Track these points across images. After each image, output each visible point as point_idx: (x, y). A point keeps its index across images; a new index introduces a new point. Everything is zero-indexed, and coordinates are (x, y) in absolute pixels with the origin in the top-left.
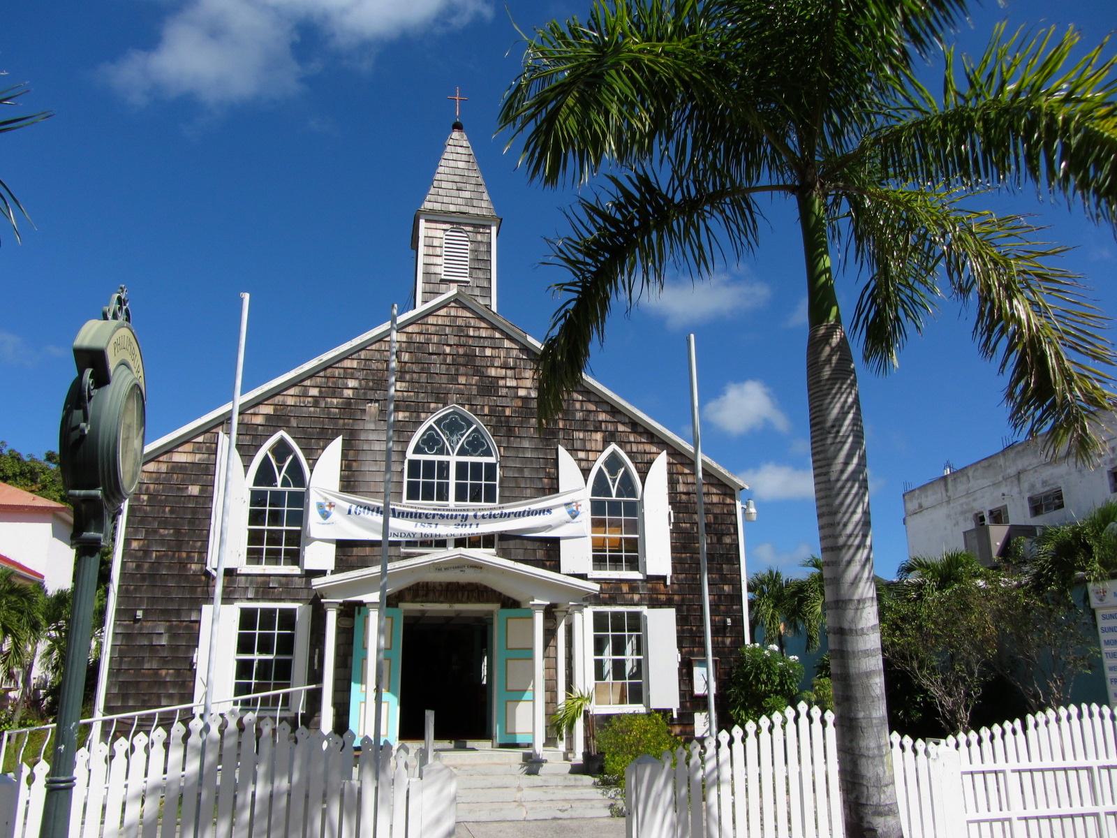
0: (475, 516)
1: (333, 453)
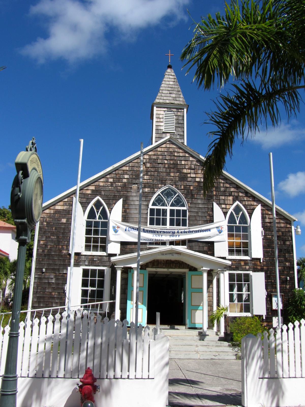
0: (178, 232)
1: (119, 206)
